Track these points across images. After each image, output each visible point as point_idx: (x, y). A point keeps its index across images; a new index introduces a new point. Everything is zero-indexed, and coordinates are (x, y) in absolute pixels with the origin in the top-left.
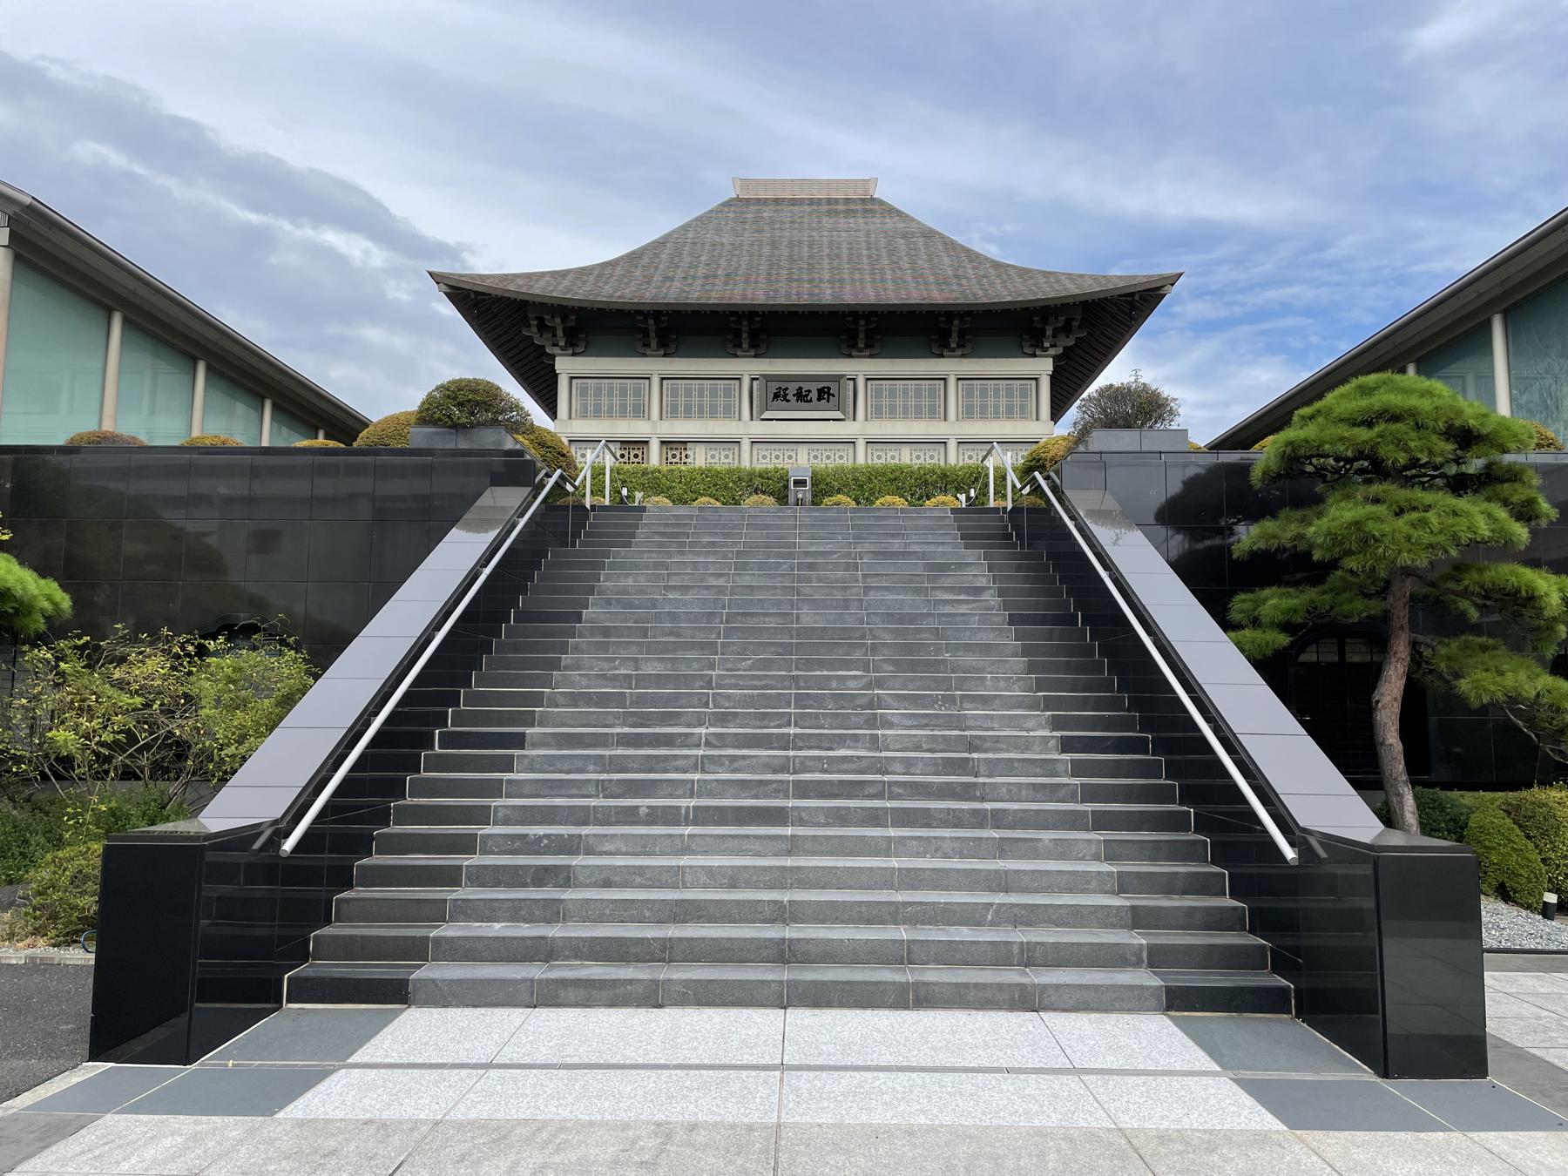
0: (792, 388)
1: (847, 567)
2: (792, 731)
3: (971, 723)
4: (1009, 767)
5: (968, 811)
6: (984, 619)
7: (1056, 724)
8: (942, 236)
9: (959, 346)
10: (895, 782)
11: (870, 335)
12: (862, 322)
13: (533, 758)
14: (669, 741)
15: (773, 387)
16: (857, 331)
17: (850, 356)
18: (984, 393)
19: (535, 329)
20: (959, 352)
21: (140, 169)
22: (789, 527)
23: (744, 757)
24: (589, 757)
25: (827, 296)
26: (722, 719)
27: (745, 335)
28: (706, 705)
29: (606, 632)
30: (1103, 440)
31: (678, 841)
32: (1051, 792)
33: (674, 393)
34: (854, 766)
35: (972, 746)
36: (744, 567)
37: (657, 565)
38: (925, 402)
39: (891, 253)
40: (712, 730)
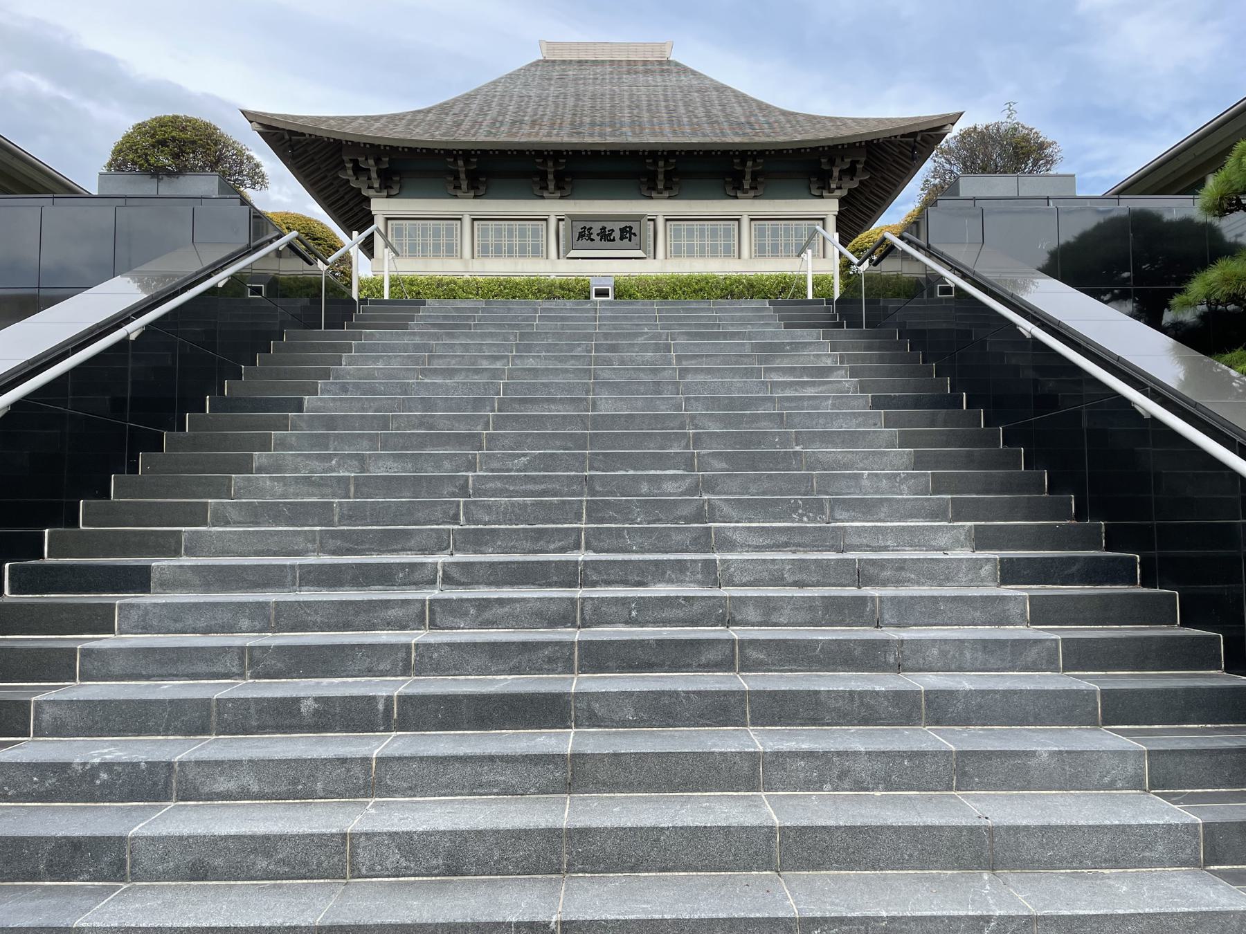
0: (596, 228)
1: (657, 348)
2: (581, 556)
3: (855, 540)
5: (886, 694)
6: (840, 401)
7: (982, 540)
8: (734, 91)
9: (752, 188)
10: (753, 643)
11: (669, 176)
12: (661, 163)
13: (146, 610)
14: (384, 576)
15: (579, 226)
16: (655, 174)
17: (650, 198)
18: (775, 233)
19: (350, 172)
20: (752, 194)
21: (64, 94)
22: (588, 319)
23: (501, 602)
24: (241, 605)
25: (628, 136)
26: (475, 540)
27: (551, 177)
28: (455, 519)
29: (330, 423)
30: (971, 186)
31: (357, 770)
32: (1012, 655)
34: (680, 613)
35: (862, 575)
36: (529, 348)
37: (417, 348)
38: (721, 242)
39: (686, 104)
40: (459, 557)
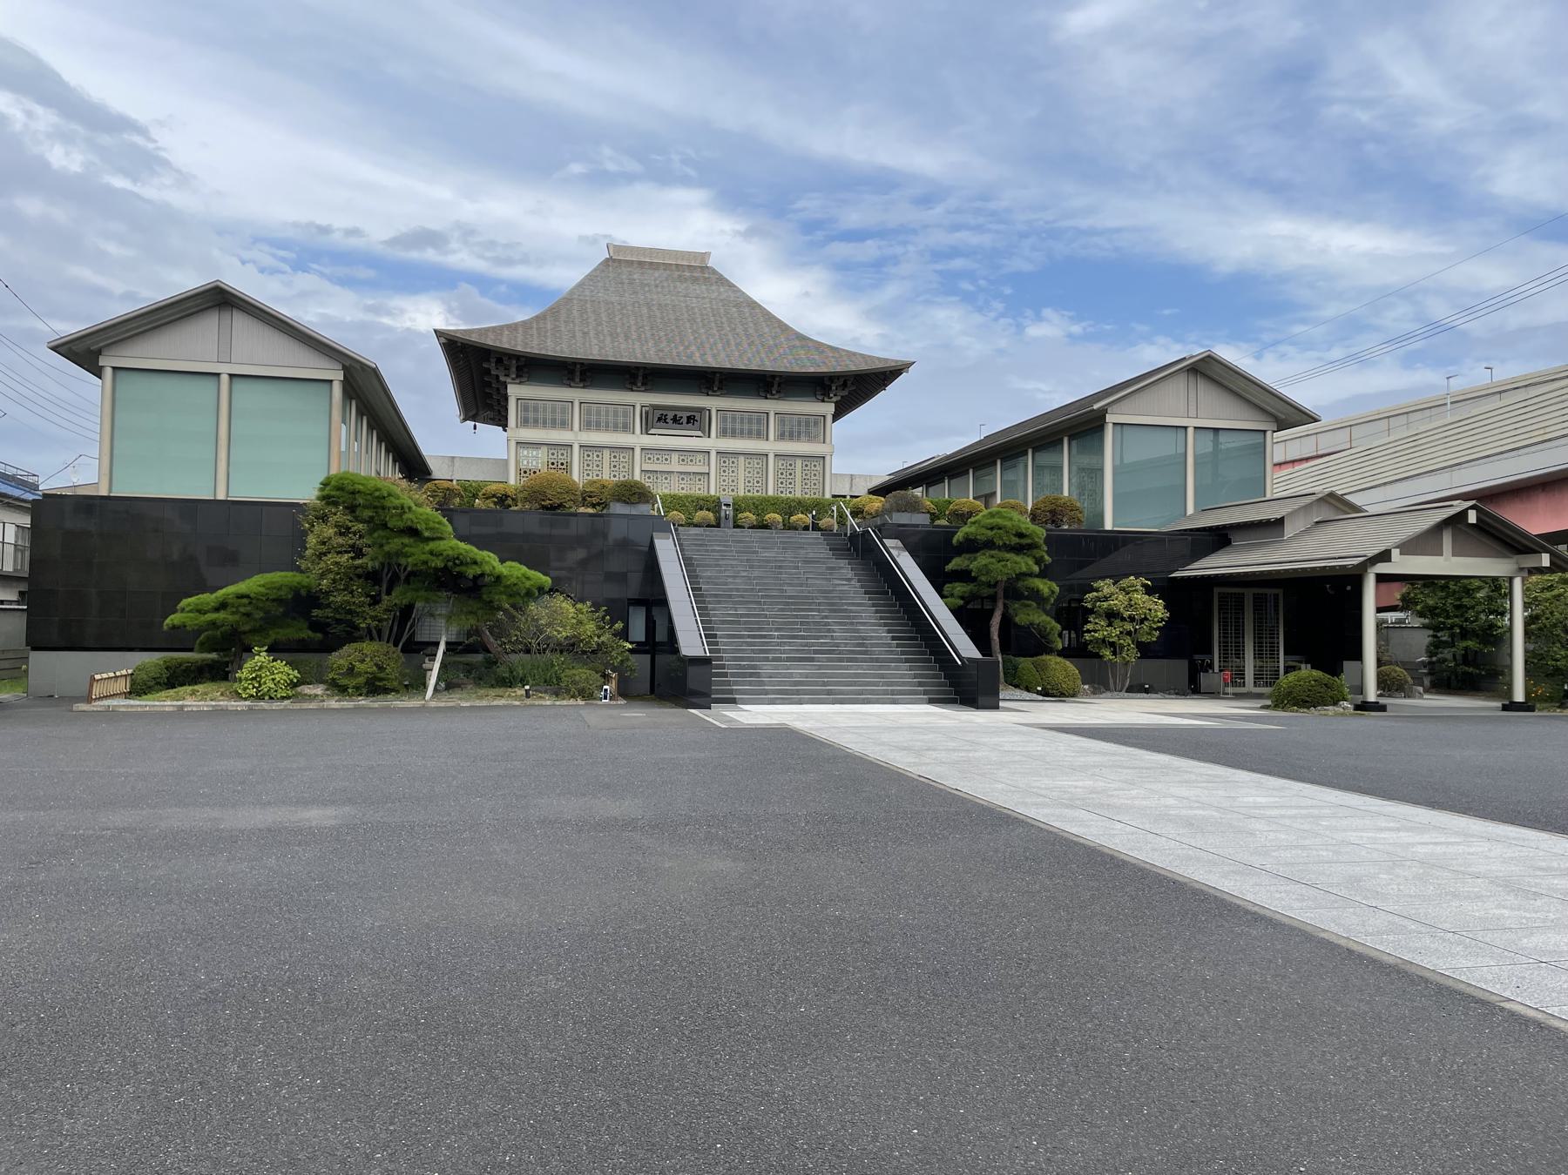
0: (671, 415)
4: (877, 645)
7: (889, 632)
15: (658, 413)
33: (589, 413)
35: (864, 638)
